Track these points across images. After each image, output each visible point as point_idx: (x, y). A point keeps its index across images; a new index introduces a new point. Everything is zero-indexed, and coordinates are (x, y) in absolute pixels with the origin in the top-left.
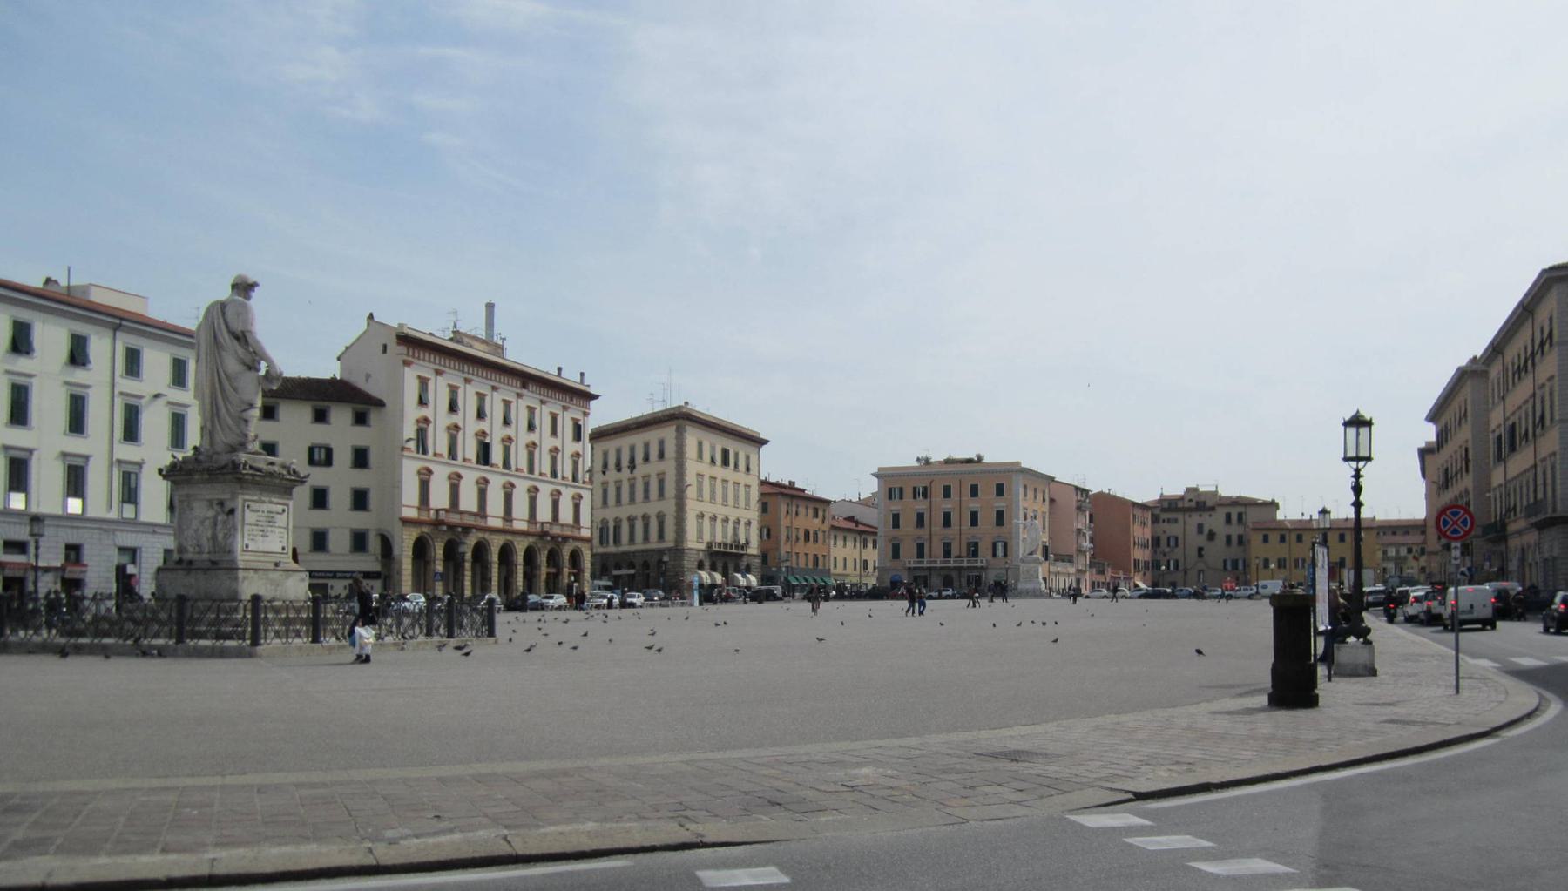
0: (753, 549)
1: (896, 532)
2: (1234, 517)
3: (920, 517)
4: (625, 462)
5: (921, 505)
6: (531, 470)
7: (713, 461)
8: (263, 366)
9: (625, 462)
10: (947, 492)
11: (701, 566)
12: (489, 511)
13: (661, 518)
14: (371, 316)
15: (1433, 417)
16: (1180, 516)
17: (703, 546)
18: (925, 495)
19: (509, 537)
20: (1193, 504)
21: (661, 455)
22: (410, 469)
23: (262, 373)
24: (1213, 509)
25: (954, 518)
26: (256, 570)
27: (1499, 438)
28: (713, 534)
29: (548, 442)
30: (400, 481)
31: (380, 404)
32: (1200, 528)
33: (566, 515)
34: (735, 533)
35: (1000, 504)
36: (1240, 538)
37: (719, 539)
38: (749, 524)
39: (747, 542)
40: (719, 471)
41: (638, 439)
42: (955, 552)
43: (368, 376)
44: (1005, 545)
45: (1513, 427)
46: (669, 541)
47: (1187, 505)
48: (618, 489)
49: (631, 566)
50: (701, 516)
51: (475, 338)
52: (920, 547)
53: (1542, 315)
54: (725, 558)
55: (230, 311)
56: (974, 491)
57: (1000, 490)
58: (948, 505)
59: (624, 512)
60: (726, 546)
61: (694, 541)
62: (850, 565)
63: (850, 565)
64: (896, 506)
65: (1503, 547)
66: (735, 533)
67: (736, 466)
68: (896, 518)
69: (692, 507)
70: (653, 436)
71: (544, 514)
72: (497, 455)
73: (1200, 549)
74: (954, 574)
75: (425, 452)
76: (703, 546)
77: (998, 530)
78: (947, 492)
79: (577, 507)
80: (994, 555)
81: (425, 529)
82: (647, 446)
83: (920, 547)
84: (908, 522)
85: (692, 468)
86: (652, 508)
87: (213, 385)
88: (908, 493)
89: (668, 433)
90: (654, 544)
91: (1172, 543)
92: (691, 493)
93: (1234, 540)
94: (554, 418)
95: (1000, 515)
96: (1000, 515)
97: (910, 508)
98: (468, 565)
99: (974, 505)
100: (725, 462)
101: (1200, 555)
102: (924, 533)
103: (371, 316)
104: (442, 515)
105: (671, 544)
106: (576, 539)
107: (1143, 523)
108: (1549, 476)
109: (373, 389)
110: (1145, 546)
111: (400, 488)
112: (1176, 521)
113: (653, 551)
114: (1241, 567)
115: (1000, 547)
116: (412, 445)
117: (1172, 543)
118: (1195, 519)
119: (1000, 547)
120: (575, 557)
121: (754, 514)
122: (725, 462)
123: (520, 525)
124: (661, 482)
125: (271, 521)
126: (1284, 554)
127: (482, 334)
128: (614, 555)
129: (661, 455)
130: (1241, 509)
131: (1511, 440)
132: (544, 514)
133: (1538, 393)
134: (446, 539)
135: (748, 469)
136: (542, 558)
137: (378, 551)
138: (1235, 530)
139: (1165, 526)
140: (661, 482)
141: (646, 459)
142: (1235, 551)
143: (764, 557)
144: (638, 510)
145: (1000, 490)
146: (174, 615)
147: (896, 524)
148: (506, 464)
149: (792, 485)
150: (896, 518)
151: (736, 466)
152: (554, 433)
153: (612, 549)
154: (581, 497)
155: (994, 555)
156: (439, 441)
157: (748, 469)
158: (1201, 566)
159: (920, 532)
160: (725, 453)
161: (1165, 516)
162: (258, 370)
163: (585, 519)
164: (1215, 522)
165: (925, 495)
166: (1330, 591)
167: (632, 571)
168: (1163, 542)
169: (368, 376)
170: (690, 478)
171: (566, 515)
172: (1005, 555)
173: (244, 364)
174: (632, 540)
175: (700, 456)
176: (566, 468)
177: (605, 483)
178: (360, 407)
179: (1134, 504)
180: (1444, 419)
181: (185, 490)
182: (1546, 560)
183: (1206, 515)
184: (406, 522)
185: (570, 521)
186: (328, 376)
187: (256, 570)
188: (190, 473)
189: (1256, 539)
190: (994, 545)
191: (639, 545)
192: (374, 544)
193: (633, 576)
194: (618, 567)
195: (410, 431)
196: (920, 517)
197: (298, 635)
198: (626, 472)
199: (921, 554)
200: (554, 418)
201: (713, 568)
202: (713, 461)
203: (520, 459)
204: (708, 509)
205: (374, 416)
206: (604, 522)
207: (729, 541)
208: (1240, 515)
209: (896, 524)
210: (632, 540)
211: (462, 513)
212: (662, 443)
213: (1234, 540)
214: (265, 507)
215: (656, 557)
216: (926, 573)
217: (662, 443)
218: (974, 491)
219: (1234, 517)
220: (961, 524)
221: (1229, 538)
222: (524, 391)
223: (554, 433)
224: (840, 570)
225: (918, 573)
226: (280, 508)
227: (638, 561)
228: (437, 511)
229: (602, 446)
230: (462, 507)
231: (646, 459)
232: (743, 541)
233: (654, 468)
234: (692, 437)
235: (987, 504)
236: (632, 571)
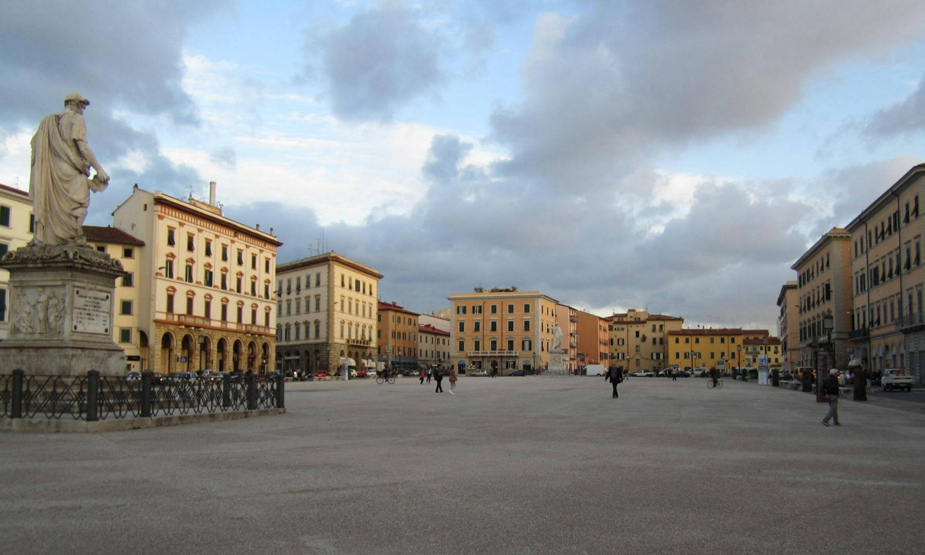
0: (374, 344)
1: (461, 334)
2: (658, 328)
3: (477, 325)
4: (294, 287)
5: (478, 317)
6: (239, 290)
7: (350, 287)
8: (93, 172)
9: (294, 287)
10: (494, 309)
11: (342, 354)
12: (212, 316)
13: (317, 323)
14: (136, 186)
15: (796, 267)
16: (625, 326)
17: (344, 342)
18: (480, 312)
19: (225, 334)
20: (633, 320)
21: (318, 284)
22: (161, 286)
23: (91, 178)
24: (644, 322)
25: (498, 326)
26: (83, 349)
27: (863, 276)
28: (350, 335)
29: (251, 273)
30: (155, 296)
31: (141, 244)
32: (637, 334)
33: (261, 320)
34: (363, 334)
35: (527, 317)
36: (661, 340)
37: (353, 337)
38: (371, 328)
39: (370, 340)
40: (353, 294)
41: (303, 274)
42: (498, 346)
43: (133, 226)
44: (530, 342)
45: (876, 269)
46: (322, 339)
47: (629, 319)
48: (289, 306)
49: (297, 354)
50: (343, 322)
51: (203, 203)
52: (477, 344)
53: (908, 197)
54: (358, 349)
55: (64, 121)
56: (511, 309)
57: (527, 309)
58: (494, 318)
59: (292, 320)
60: (357, 342)
61: (338, 338)
62: (429, 354)
63: (429, 354)
64: (462, 318)
65: (867, 346)
66: (363, 334)
67: (364, 292)
68: (462, 325)
69: (338, 316)
70: (312, 272)
71: (247, 319)
72: (217, 280)
73: (637, 346)
74: (498, 360)
75: (171, 276)
76: (344, 342)
77: (526, 333)
78: (494, 309)
79: (267, 315)
80: (523, 349)
81: (172, 328)
82: (308, 277)
83: (477, 344)
84: (469, 327)
85: (338, 292)
86: (311, 318)
87: (47, 186)
88: (469, 310)
89: (323, 269)
90: (312, 340)
91: (621, 342)
92: (337, 307)
93: (658, 341)
94: (254, 259)
95: (527, 324)
96: (527, 324)
97: (470, 319)
98: (197, 352)
99: (511, 317)
100: (358, 289)
101: (637, 351)
102: (479, 334)
103: (136, 186)
104: (183, 319)
105: (324, 340)
106: (266, 335)
107: (605, 330)
108: (915, 300)
109: (138, 235)
110: (605, 344)
111: (154, 300)
112: (623, 329)
113: (311, 344)
114: (661, 357)
115: (527, 344)
116: (163, 271)
117: (621, 342)
118: (634, 329)
119: (527, 344)
120: (265, 346)
121: (374, 322)
122: (358, 289)
123: (232, 326)
124: (318, 301)
125: (96, 306)
126: (689, 350)
127: (207, 201)
128: (304, 345)
129: (318, 284)
130: (662, 323)
131: (876, 278)
132: (247, 319)
133: (904, 248)
134: (184, 334)
135: (371, 293)
136: (244, 349)
137: (138, 342)
138: (658, 335)
139: (616, 332)
140: (318, 301)
141: (308, 286)
142: (658, 348)
143: (379, 349)
144: (301, 319)
145: (527, 309)
146: (10, 388)
147: (462, 329)
148: (224, 286)
149: (394, 305)
150: (462, 325)
151: (364, 292)
152: (254, 266)
153: (284, 343)
154: (270, 309)
155: (523, 349)
156: (179, 270)
157: (371, 293)
158: (638, 357)
159: (477, 334)
160: (358, 282)
161: (615, 326)
162: (88, 175)
163: (273, 323)
164: (646, 330)
165: (480, 312)
166: (384, 374)
167: (298, 357)
168: (615, 342)
169: (133, 226)
170: (337, 298)
171: (261, 320)
172: (530, 349)
173: (77, 169)
174: (297, 338)
175: (343, 285)
176: (260, 290)
177: (289, 301)
178: (128, 247)
179: (600, 318)
180: (804, 269)
181: (20, 277)
182: (912, 354)
183: (640, 326)
184: (157, 322)
185: (263, 324)
186: (105, 225)
187: (83, 349)
188: (24, 261)
189: (672, 340)
190: (523, 342)
191: (302, 340)
192: (135, 337)
193: (298, 360)
194: (288, 354)
195: (161, 262)
196: (477, 325)
197: (130, 408)
198: (293, 295)
199: (477, 348)
200: (254, 259)
201: (350, 355)
202: (350, 287)
203: (232, 283)
204: (346, 317)
205: (136, 252)
206: (288, 326)
207: (359, 338)
208: (661, 327)
209: (462, 329)
210: (297, 338)
211: (195, 317)
212: (318, 275)
213: (658, 341)
214: (91, 294)
215: (314, 349)
216: (480, 360)
217: (318, 275)
218: (511, 309)
219: (658, 328)
220: (502, 328)
221: (654, 340)
222: (236, 239)
223: (254, 266)
224: (423, 357)
225: (475, 360)
226: (104, 295)
227: (302, 351)
228: (179, 315)
229: (285, 277)
230: (195, 313)
231: (308, 286)
232: (367, 338)
233: (312, 292)
234: (338, 270)
235: (519, 317)
236: (298, 357)
